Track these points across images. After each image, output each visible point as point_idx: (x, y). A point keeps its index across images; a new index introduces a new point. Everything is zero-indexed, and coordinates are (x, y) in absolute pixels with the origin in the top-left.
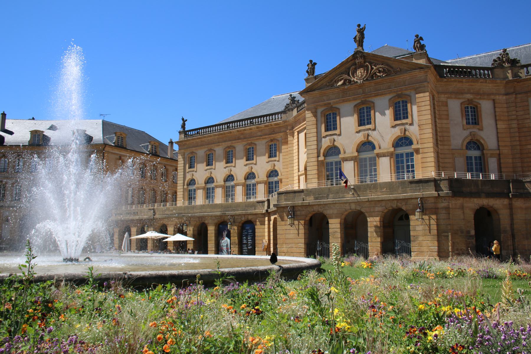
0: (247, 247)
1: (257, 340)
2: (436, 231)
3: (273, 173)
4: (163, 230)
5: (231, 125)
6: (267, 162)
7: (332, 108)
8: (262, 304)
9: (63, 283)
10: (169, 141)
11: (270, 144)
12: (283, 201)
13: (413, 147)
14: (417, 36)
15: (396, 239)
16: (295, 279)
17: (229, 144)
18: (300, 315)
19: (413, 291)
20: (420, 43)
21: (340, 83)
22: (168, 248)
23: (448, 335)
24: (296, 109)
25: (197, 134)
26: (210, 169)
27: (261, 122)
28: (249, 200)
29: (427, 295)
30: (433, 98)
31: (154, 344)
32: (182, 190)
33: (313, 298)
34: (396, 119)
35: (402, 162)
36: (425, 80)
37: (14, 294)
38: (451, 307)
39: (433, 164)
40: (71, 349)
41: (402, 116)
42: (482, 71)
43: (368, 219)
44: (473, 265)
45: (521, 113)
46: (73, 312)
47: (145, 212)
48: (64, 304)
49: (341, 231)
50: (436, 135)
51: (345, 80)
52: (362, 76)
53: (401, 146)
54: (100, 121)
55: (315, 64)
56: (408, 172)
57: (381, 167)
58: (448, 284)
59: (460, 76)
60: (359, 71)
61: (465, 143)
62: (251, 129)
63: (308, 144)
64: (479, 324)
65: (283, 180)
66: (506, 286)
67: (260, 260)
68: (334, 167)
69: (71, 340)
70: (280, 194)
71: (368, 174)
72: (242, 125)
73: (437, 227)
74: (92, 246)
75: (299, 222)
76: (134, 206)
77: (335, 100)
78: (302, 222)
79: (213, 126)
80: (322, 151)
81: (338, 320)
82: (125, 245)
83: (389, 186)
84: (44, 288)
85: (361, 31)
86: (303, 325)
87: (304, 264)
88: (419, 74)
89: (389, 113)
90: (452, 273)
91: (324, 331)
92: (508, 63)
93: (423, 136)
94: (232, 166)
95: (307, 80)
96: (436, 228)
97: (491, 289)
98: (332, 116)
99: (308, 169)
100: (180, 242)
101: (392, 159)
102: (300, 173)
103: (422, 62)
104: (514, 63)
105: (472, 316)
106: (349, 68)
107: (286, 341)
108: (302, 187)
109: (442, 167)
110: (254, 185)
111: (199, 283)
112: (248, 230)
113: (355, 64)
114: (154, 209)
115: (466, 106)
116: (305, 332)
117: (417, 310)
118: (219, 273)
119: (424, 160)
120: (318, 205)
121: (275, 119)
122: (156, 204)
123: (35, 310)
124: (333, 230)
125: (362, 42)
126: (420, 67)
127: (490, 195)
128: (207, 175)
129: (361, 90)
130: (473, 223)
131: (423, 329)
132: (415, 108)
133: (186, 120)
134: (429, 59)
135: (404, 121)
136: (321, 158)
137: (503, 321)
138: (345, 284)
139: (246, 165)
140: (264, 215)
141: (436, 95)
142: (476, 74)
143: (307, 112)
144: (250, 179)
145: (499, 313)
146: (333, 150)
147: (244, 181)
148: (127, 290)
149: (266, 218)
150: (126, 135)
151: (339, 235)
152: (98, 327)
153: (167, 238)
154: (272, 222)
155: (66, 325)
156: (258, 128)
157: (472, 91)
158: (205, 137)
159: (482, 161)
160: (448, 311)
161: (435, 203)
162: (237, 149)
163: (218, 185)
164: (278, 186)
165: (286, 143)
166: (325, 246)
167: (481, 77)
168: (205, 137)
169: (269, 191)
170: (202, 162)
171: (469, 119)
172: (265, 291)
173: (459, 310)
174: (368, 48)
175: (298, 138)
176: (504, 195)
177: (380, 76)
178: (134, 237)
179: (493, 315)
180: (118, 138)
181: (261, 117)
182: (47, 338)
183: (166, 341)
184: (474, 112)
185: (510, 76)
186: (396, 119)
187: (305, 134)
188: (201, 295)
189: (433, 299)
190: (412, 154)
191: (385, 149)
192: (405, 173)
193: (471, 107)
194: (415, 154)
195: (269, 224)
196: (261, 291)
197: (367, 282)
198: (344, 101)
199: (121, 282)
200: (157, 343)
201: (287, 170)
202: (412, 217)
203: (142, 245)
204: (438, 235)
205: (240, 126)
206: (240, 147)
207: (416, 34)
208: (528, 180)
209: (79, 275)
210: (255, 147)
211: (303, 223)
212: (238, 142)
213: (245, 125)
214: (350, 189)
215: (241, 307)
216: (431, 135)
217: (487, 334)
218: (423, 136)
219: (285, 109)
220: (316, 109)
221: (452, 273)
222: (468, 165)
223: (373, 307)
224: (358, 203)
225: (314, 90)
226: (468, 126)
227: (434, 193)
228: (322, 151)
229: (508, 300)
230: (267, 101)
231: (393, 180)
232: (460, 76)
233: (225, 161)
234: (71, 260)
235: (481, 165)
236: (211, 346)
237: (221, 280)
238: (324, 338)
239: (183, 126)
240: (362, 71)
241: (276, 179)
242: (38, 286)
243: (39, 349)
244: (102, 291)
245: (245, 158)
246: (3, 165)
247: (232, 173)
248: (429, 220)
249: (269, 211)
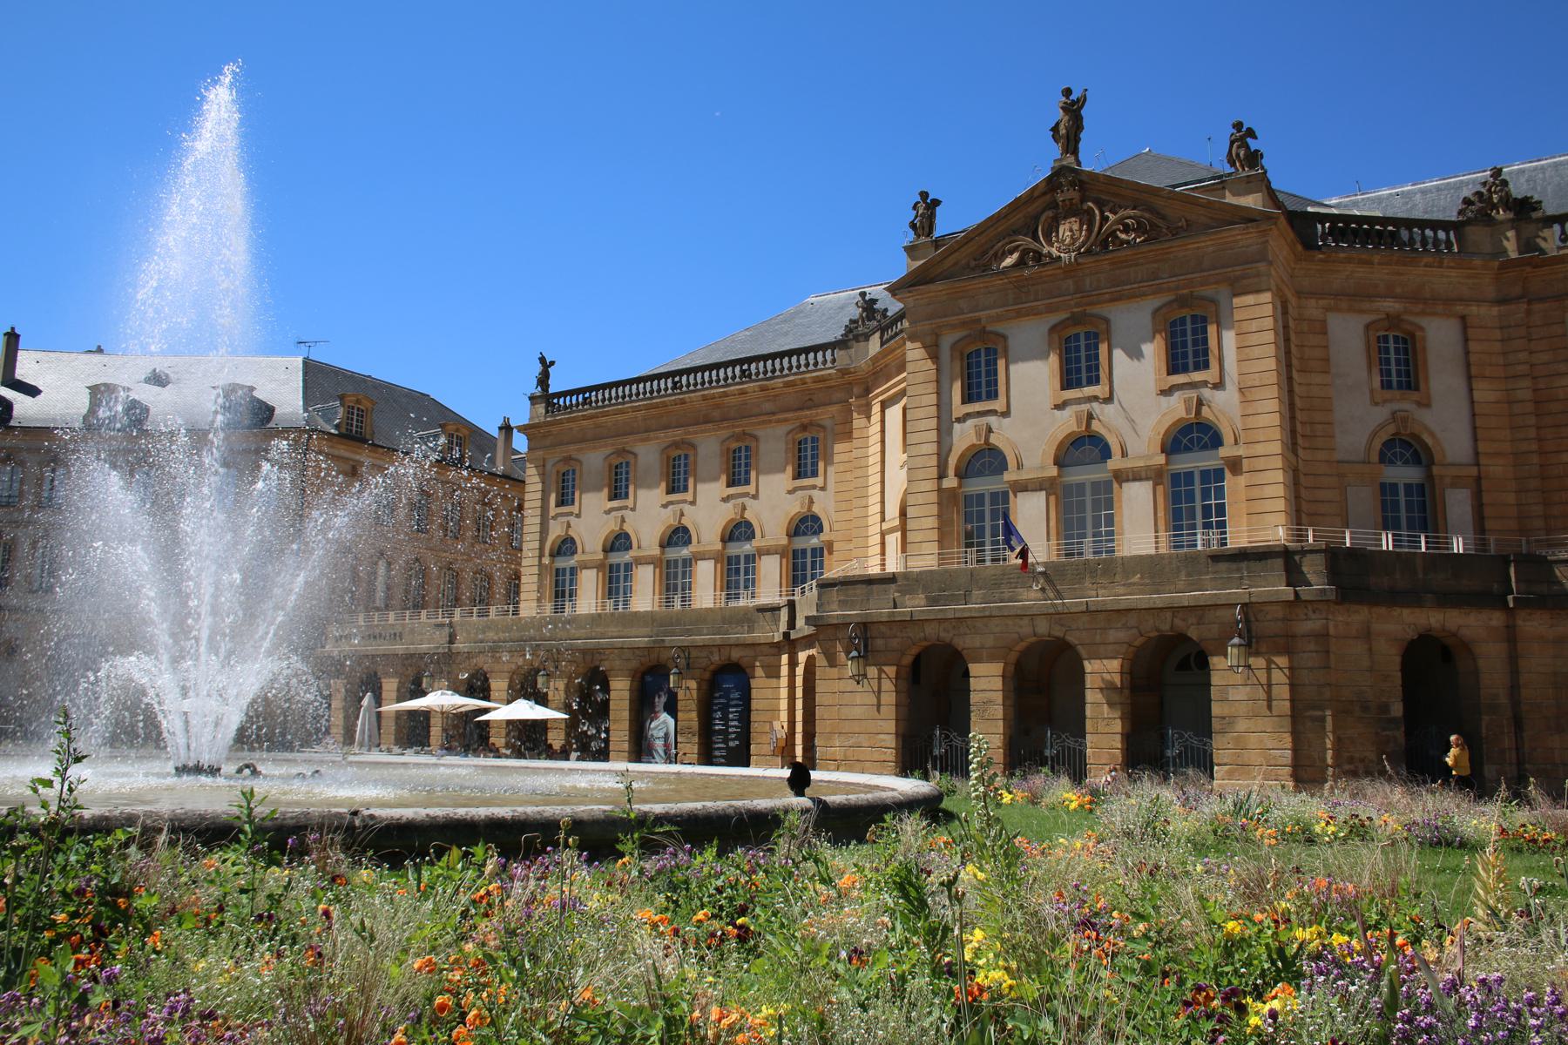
0: (726, 741)
1: (734, 1016)
2: (1288, 704)
3: (807, 524)
4: (478, 687)
5: (684, 378)
6: (790, 492)
7: (984, 333)
8: (758, 910)
9: (162, 838)
10: (500, 423)
11: (800, 436)
12: (835, 606)
13: (1224, 452)
14: (1238, 126)
15: (1168, 726)
16: (861, 840)
17: (677, 434)
18: (869, 945)
19: (1210, 881)
20: (1248, 147)
21: (1009, 261)
22: (492, 740)
23: (1309, 1013)
24: (877, 335)
25: (584, 403)
26: (620, 509)
27: (773, 371)
28: (732, 604)
29: (1253, 892)
30: (1283, 308)
31: (425, 1020)
32: (536, 570)
33: (906, 896)
34: (1173, 369)
35: (1190, 497)
36: (1262, 256)
37: (11, 867)
38: (1323, 929)
39: (1281, 505)
40: (174, 1034)
41: (1191, 360)
42: (1429, 232)
43: (1086, 663)
44: (1394, 808)
45: (1545, 357)
46: (188, 925)
47: (423, 633)
48: (162, 900)
49: (1005, 698)
50: (1293, 418)
51: (1025, 253)
52: (1074, 240)
53: (1188, 449)
54: (298, 361)
55: (936, 203)
56: (1207, 526)
57: (1126, 511)
58: (1316, 860)
59: (1364, 244)
60: (1067, 226)
61: (1377, 445)
62: (743, 392)
63: (911, 439)
64: (1404, 981)
65: (836, 546)
66: (1487, 869)
67: (760, 782)
68: (987, 508)
69: (173, 1009)
70: (825, 586)
71: (1089, 530)
72: (718, 381)
73: (1292, 691)
74: (268, 730)
75: (881, 671)
76: (392, 615)
77: (993, 312)
78: (891, 670)
79: (630, 382)
80: (952, 461)
81: (980, 962)
82: (363, 731)
83: (1150, 567)
84: (106, 851)
85: (1074, 109)
86: (874, 975)
87: (890, 794)
88: (1242, 238)
89: (1153, 350)
90: (1331, 829)
91: (935, 994)
92: (1507, 208)
93: (1253, 422)
94: (685, 501)
95: (911, 250)
96: (1287, 695)
97: (1443, 878)
98: (983, 359)
99: (911, 512)
100: (524, 722)
101: (1160, 489)
102: (885, 526)
103: (1252, 201)
104: (1524, 208)
105: (1384, 957)
106: (1036, 218)
107: (822, 1023)
108: (893, 566)
109: (1309, 515)
110: (750, 559)
111: (566, 846)
112: (728, 691)
113: (1054, 205)
114: (451, 625)
115: (1382, 333)
116: (877, 997)
117: (1219, 935)
118: (632, 816)
119: (1256, 493)
120: (940, 621)
121: (816, 364)
122: (458, 611)
123: (74, 915)
124: (981, 695)
125: (1077, 140)
126: (1248, 218)
127: (1448, 599)
128: (610, 525)
129: (1070, 282)
130: (1399, 682)
131: (1234, 992)
132: (1229, 338)
133: (552, 363)
134: (1272, 195)
135: (1197, 376)
136: (950, 482)
137: (1474, 974)
138: (1006, 855)
139: (726, 500)
140: (777, 648)
141: (1293, 301)
142: (1412, 240)
143: (909, 345)
144: (738, 540)
145: (1463, 948)
146: (986, 459)
147: (719, 546)
148: (355, 863)
149: (785, 658)
150: (374, 403)
151: (998, 711)
152: (262, 971)
153: (486, 711)
154: (800, 670)
155: (163, 962)
156: (763, 389)
157: (1398, 290)
158: (606, 414)
159: (1428, 499)
160: (1311, 941)
161: (1285, 619)
162: (701, 451)
163: (654, 551)
164: (822, 562)
165: (848, 435)
166: (958, 742)
167: (1425, 250)
168: (606, 414)
169: (795, 578)
170: (598, 489)
171: (1389, 373)
172: (766, 872)
173: (1347, 938)
174: (1094, 158)
175: (883, 421)
176: (1491, 599)
177: (1128, 242)
178: (391, 708)
179: (1445, 957)
180: (349, 411)
181: (773, 356)
182: (99, 998)
183: (464, 1015)
184: (1406, 351)
185: (1511, 247)
186: (1173, 369)
187: (904, 409)
188: (584, 884)
189: (1270, 903)
190: (1219, 475)
191: (1140, 458)
192: (1199, 531)
193: (1396, 338)
194: (1228, 474)
195: (792, 675)
196: (754, 872)
197: (1073, 852)
198: (1019, 314)
199: (338, 838)
200: (435, 1021)
201: (847, 516)
202: (1215, 661)
203: (414, 731)
204: (1292, 716)
205: (710, 382)
206: (709, 446)
207: (1235, 120)
208: (1564, 555)
209: (218, 817)
210: (753, 445)
211: (893, 675)
212: (703, 432)
213: (726, 379)
214: (1035, 576)
215: (695, 918)
216: (1275, 419)
217: (1426, 1012)
218: (1253, 422)
219: (845, 335)
220: (937, 336)
221: (1331, 829)
222: (1384, 509)
223: (1086, 924)
224: (1056, 616)
225: (932, 281)
226: (1388, 394)
227: (1284, 591)
228: (952, 461)
229: (1494, 913)
230: (791, 309)
231: (1163, 551)
232: (1364, 244)
233: (663, 485)
234: (198, 770)
235: (1423, 510)
236: (595, 1031)
237: (636, 835)
238: (936, 1014)
239: (543, 380)
240: (1076, 227)
241: (814, 541)
242: (87, 843)
243: (74, 1034)
244: (279, 865)
245: (724, 478)
247: (685, 522)
248: (1269, 669)
249: (793, 636)
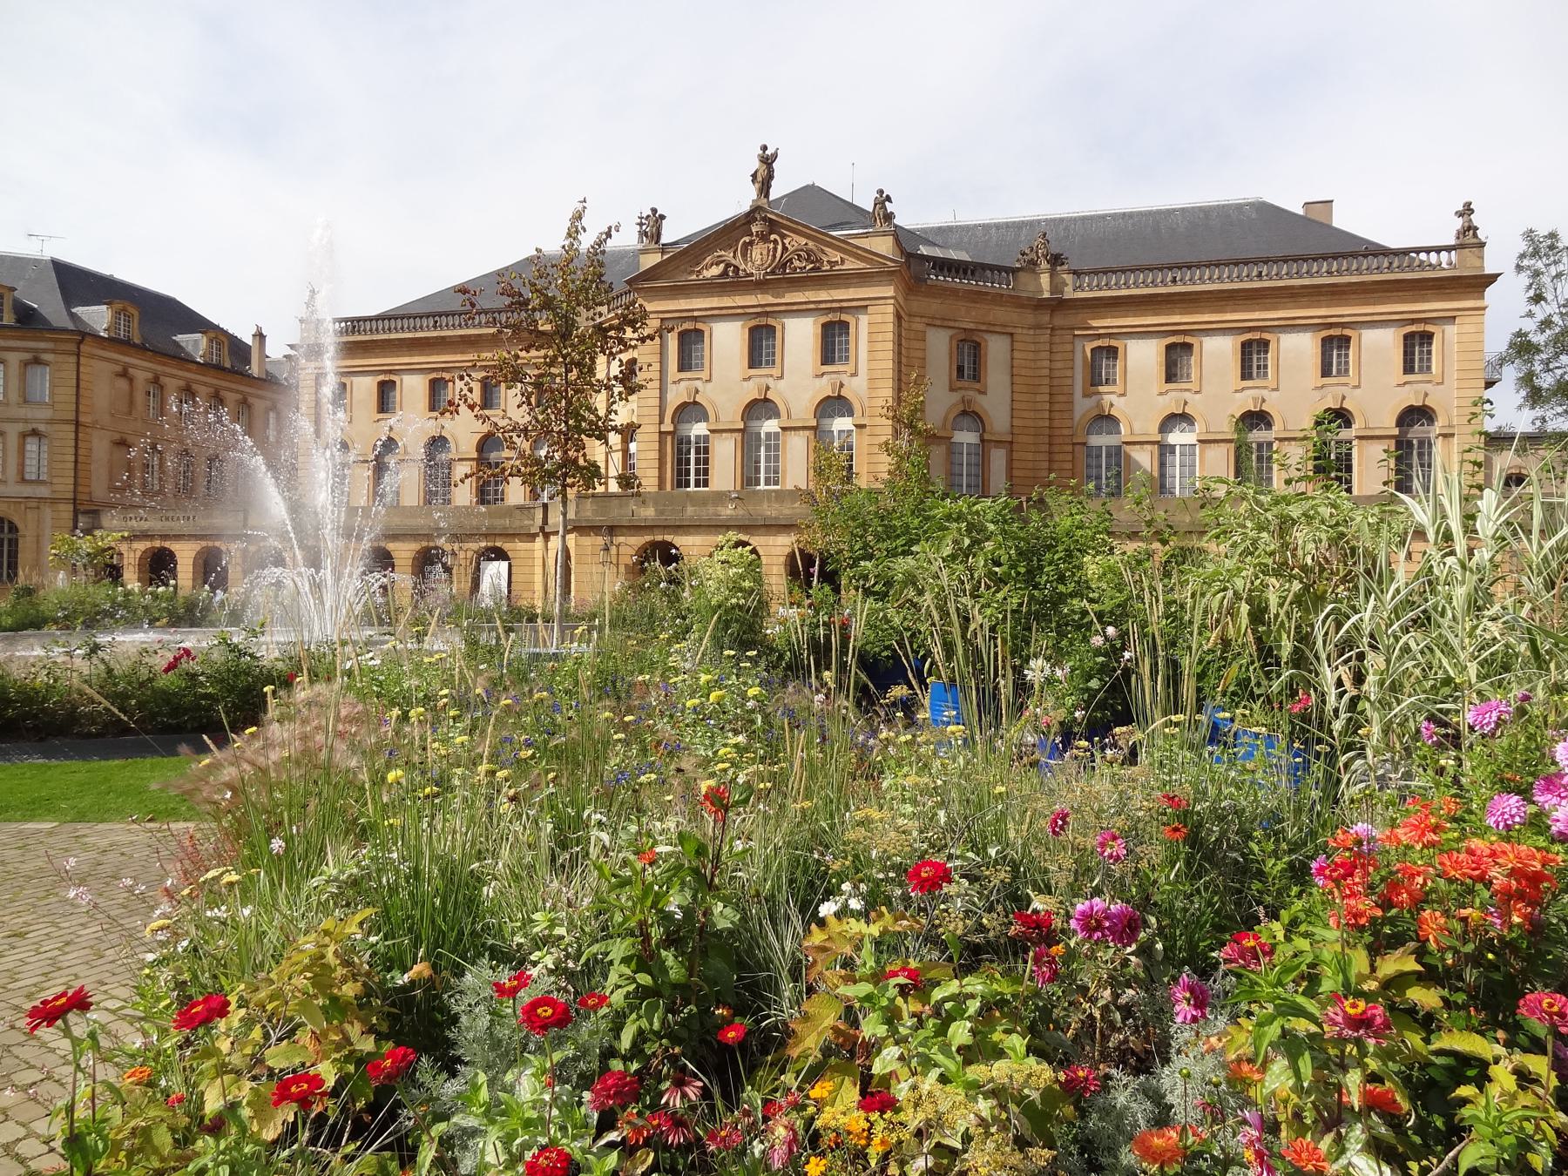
10: (254, 331)
55: (662, 217)
125: (769, 187)
246: (34, 469)
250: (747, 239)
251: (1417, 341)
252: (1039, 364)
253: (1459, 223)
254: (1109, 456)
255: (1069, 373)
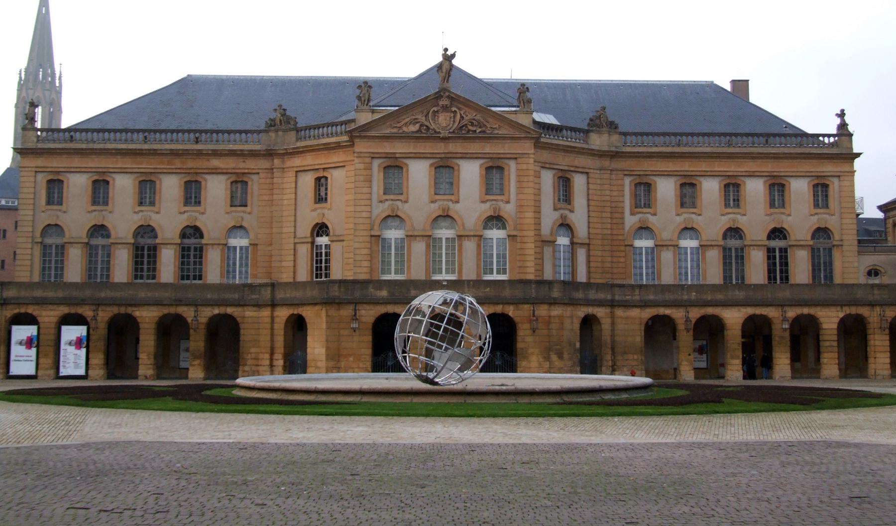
250: (435, 109)
251: (820, 188)
252: (603, 192)
253: (838, 121)
254: (647, 253)
255: (621, 199)
